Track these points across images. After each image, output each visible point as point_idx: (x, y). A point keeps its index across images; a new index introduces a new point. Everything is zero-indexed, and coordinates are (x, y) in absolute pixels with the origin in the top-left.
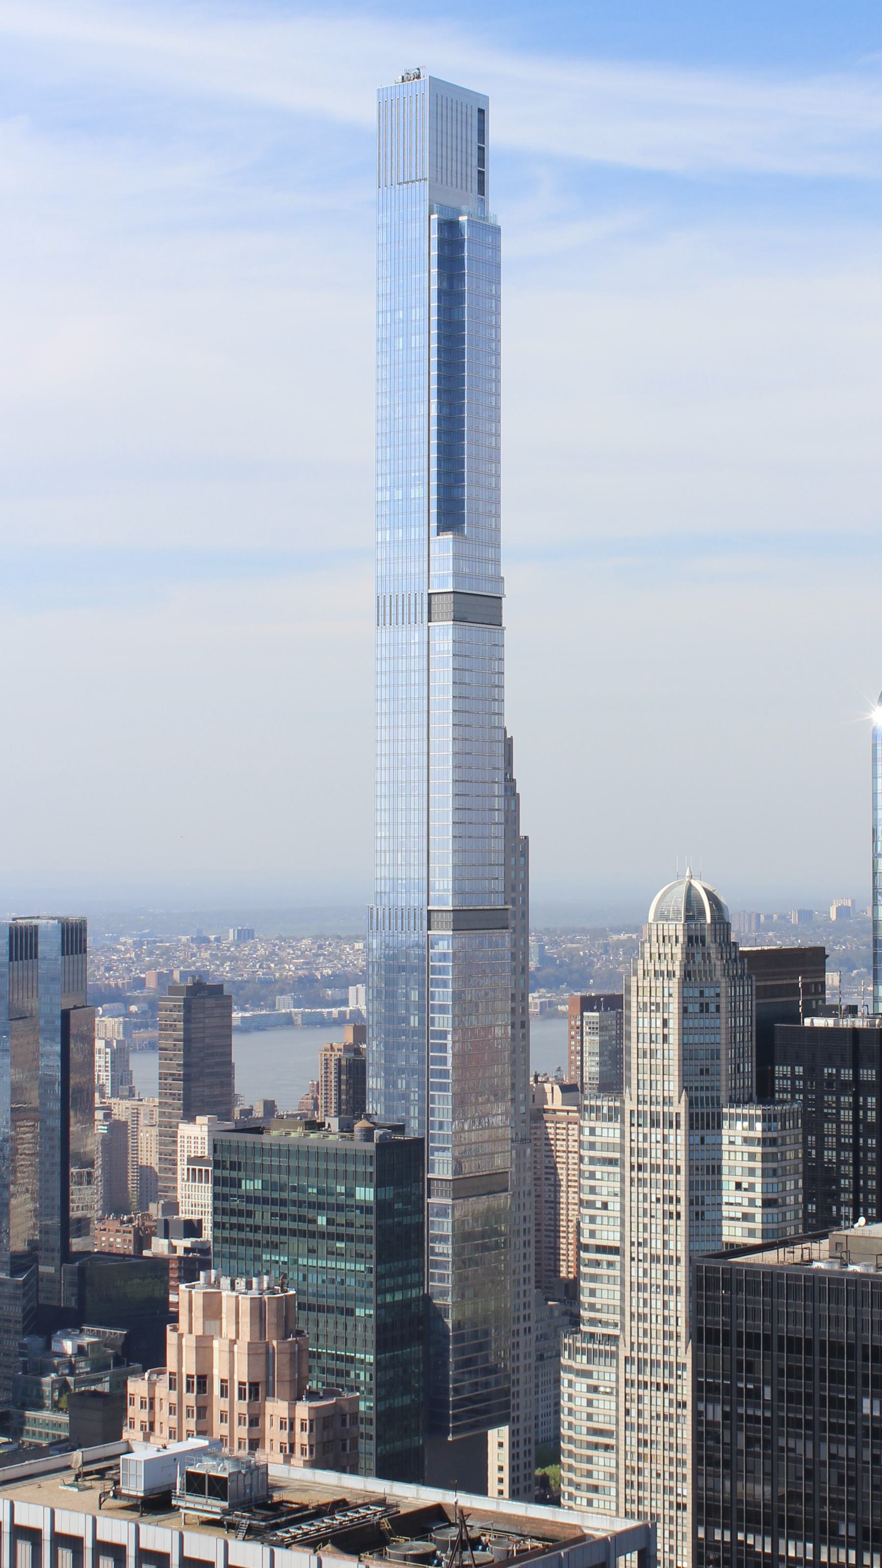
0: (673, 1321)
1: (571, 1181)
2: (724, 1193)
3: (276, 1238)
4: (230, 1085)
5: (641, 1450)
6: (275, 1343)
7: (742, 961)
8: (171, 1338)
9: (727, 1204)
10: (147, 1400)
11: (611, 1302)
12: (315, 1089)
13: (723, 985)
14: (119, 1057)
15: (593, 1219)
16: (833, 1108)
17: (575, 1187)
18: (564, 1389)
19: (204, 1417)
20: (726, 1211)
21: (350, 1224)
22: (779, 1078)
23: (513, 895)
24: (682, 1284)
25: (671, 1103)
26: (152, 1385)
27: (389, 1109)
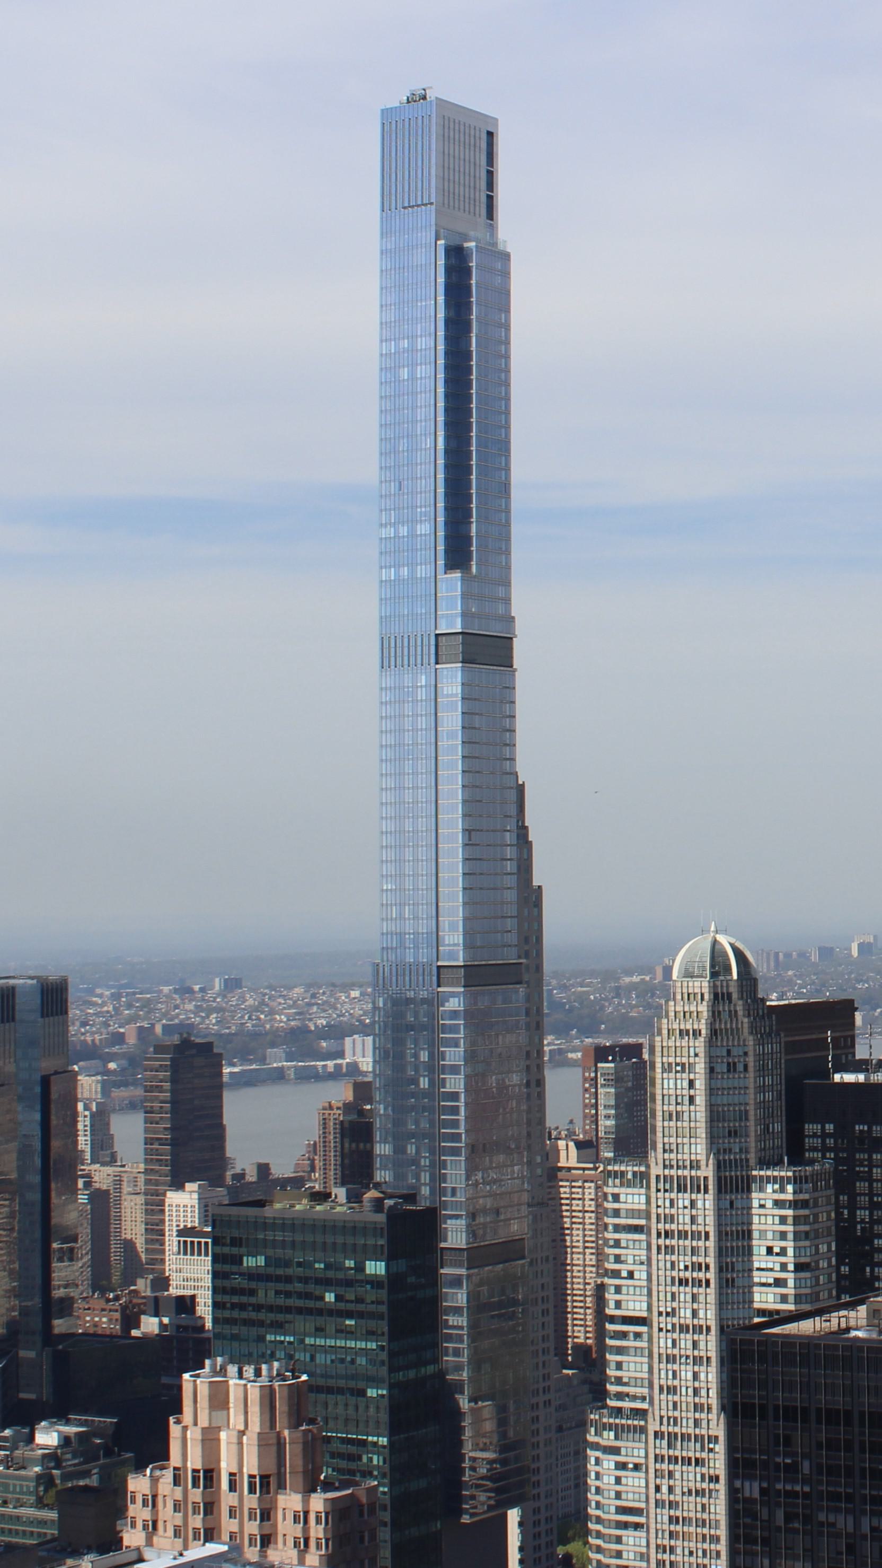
0: (703, 1392)
1: (588, 1242)
2: (755, 1258)
3: (280, 1317)
4: (222, 1148)
5: (672, 1527)
6: (286, 1433)
7: (770, 1018)
8: (175, 1430)
9: (758, 1269)
10: (150, 1497)
11: (639, 1375)
12: (311, 1149)
13: (751, 1043)
14: (100, 1121)
15: (618, 1289)
16: (866, 1166)
17: (592, 1248)
18: (592, 1467)
19: (212, 1513)
20: (757, 1277)
21: (359, 1300)
22: (809, 1136)
23: (526, 948)
24: (713, 1354)
25: (698, 1168)
26: (155, 1481)
27: (397, 1177)
